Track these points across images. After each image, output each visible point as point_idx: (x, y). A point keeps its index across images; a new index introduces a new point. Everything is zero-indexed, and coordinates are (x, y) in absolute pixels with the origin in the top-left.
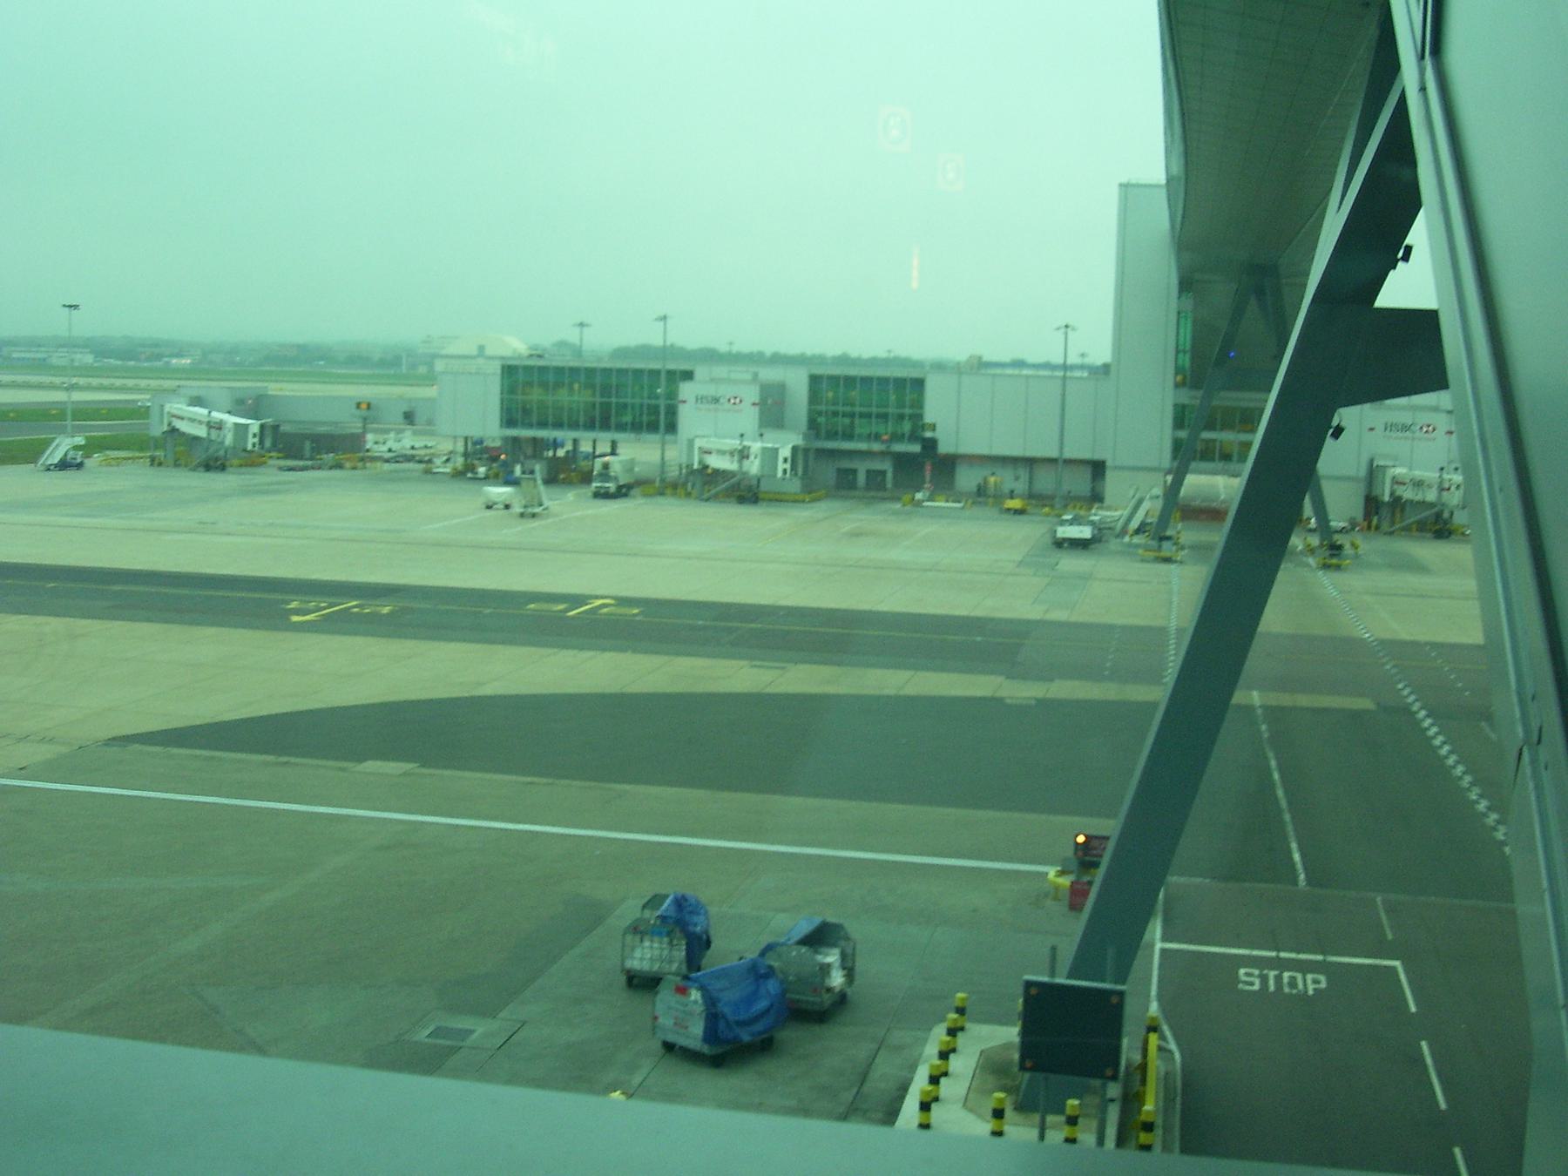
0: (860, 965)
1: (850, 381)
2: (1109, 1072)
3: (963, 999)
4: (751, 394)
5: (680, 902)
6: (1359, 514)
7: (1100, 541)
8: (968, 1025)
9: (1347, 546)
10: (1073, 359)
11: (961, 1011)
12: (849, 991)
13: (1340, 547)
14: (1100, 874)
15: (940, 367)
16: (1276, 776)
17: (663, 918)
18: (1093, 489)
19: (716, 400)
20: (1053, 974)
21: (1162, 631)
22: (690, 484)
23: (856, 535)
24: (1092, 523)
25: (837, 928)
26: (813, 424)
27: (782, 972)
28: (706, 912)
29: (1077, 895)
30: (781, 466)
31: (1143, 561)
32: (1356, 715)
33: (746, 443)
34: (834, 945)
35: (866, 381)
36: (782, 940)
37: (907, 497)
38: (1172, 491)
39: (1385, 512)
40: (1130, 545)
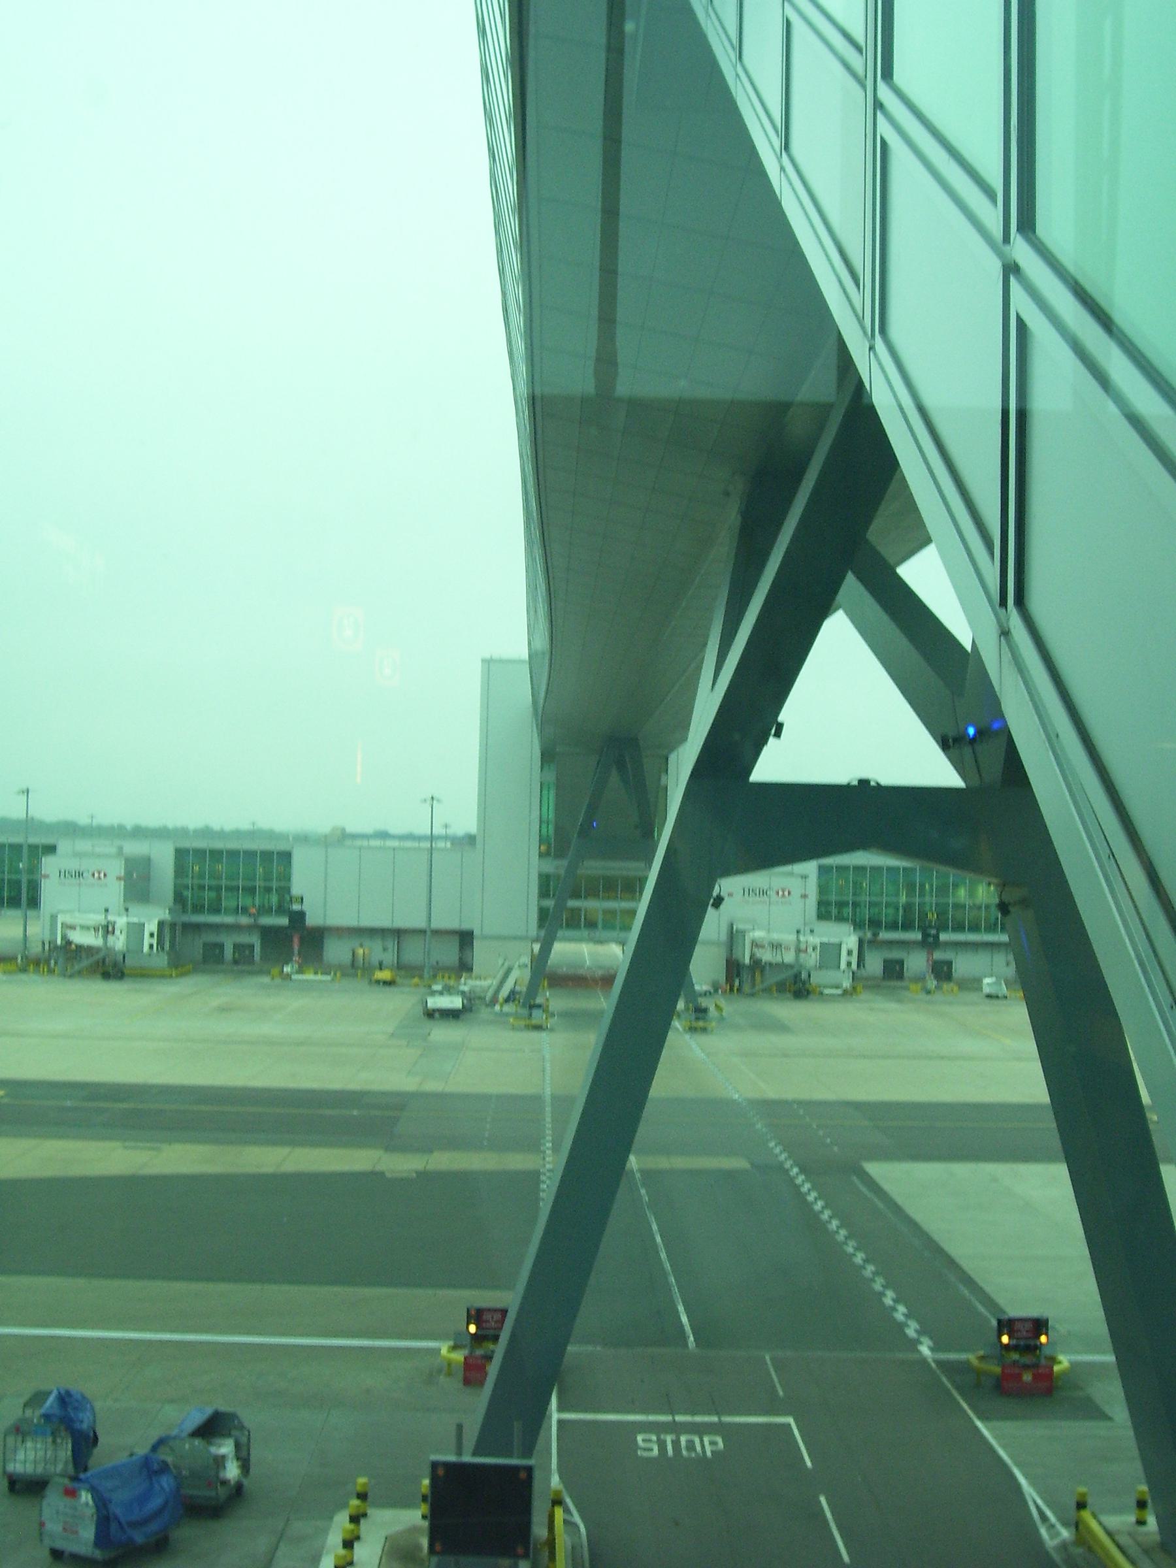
0: (255, 1454)
1: (216, 855)
2: (520, 1550)
3: (364, 1485)
4: (117, 868)
5: (64, 1399)
6: (722, 978)
7: (471, 1010)
8: (370, 1511)
9: (712, 1008)
10: (438, 830)
11: (362, 1496)
12: (245, 1482)
13: (705, 1011)
14: (499, 1350)
15: (304, 839)
16: (658, 1239)
17: (47, 1417)
18: (460, 959)
19: (80, 874)
20: (459, 1452)
21: (537, 1099)
22: (52, 962)
23: (224, 1010)
24: (463, 993)
25: (232, 1416)
26: (179, 898)
27: (175, 1467)
28: (92, 1408)
29: (473, 1373)
30: (147, 941)
31: (514, 1028)
32: (730, 1174)
33: (111, 918)
34: (229, 1435)
35: (233, 854)
36: (175, 1432)
37: (275, 971)
38: (539, 962)
39: (745, 975)
40: (502, 1014)
